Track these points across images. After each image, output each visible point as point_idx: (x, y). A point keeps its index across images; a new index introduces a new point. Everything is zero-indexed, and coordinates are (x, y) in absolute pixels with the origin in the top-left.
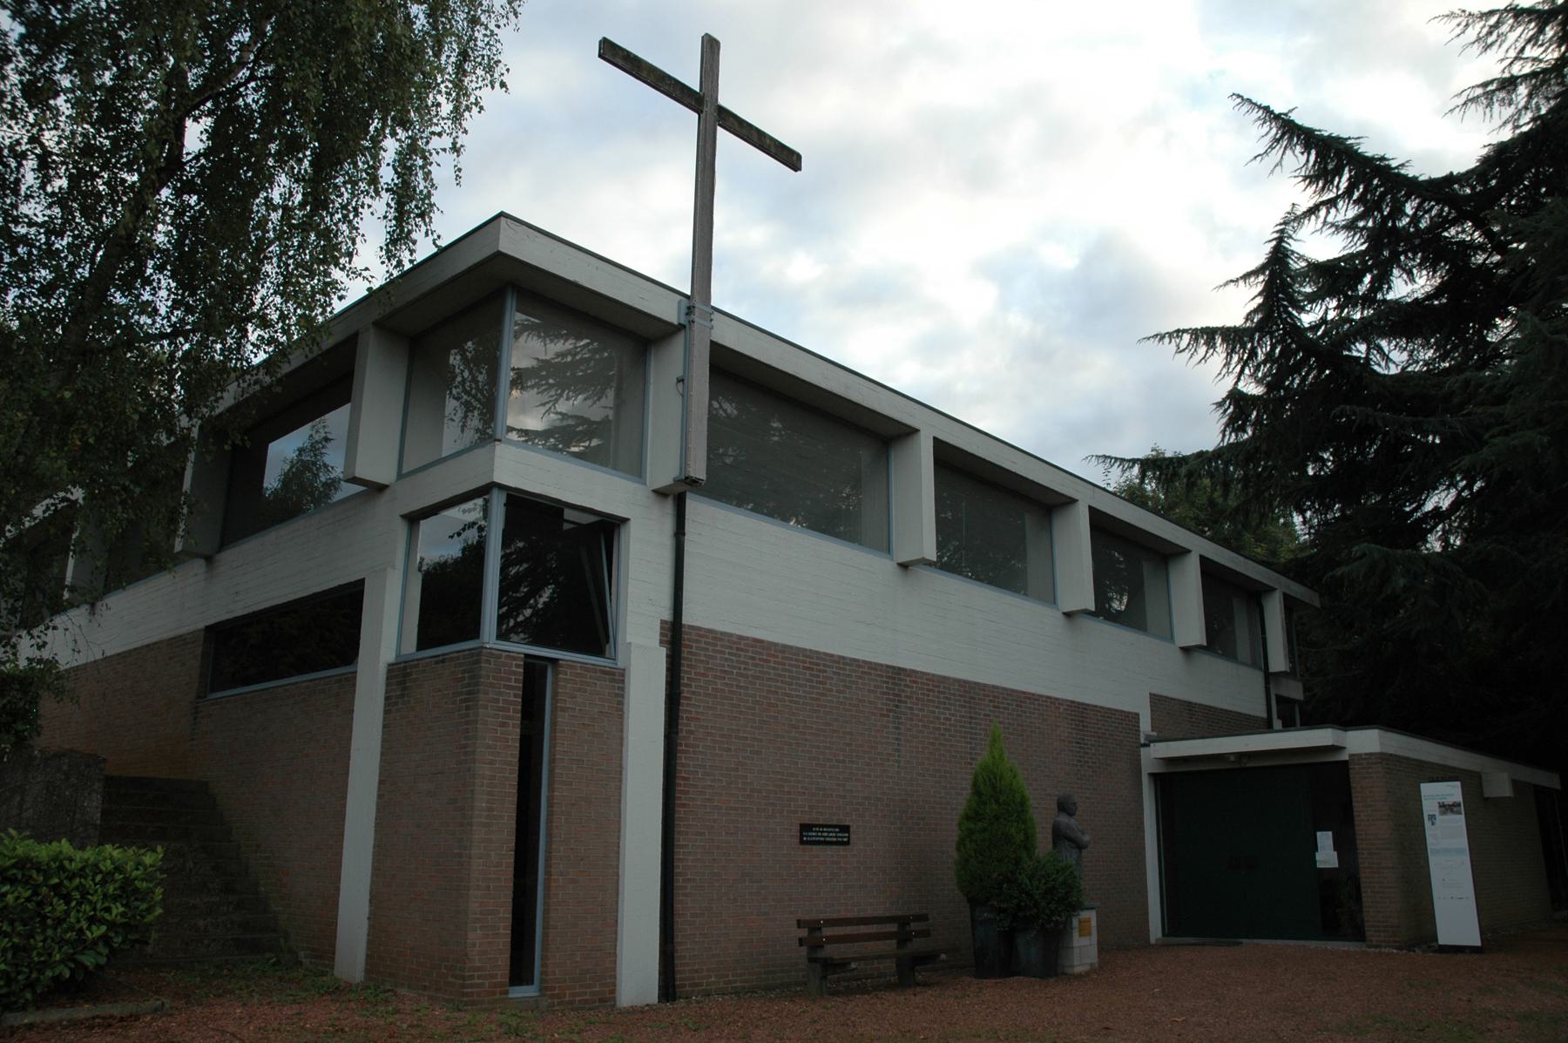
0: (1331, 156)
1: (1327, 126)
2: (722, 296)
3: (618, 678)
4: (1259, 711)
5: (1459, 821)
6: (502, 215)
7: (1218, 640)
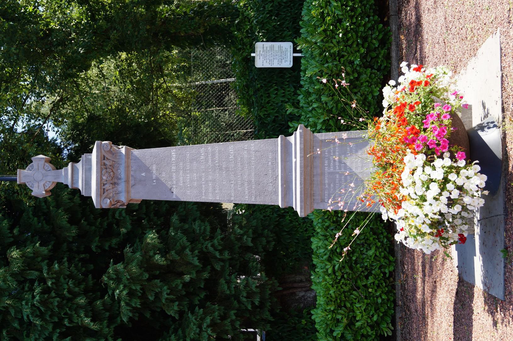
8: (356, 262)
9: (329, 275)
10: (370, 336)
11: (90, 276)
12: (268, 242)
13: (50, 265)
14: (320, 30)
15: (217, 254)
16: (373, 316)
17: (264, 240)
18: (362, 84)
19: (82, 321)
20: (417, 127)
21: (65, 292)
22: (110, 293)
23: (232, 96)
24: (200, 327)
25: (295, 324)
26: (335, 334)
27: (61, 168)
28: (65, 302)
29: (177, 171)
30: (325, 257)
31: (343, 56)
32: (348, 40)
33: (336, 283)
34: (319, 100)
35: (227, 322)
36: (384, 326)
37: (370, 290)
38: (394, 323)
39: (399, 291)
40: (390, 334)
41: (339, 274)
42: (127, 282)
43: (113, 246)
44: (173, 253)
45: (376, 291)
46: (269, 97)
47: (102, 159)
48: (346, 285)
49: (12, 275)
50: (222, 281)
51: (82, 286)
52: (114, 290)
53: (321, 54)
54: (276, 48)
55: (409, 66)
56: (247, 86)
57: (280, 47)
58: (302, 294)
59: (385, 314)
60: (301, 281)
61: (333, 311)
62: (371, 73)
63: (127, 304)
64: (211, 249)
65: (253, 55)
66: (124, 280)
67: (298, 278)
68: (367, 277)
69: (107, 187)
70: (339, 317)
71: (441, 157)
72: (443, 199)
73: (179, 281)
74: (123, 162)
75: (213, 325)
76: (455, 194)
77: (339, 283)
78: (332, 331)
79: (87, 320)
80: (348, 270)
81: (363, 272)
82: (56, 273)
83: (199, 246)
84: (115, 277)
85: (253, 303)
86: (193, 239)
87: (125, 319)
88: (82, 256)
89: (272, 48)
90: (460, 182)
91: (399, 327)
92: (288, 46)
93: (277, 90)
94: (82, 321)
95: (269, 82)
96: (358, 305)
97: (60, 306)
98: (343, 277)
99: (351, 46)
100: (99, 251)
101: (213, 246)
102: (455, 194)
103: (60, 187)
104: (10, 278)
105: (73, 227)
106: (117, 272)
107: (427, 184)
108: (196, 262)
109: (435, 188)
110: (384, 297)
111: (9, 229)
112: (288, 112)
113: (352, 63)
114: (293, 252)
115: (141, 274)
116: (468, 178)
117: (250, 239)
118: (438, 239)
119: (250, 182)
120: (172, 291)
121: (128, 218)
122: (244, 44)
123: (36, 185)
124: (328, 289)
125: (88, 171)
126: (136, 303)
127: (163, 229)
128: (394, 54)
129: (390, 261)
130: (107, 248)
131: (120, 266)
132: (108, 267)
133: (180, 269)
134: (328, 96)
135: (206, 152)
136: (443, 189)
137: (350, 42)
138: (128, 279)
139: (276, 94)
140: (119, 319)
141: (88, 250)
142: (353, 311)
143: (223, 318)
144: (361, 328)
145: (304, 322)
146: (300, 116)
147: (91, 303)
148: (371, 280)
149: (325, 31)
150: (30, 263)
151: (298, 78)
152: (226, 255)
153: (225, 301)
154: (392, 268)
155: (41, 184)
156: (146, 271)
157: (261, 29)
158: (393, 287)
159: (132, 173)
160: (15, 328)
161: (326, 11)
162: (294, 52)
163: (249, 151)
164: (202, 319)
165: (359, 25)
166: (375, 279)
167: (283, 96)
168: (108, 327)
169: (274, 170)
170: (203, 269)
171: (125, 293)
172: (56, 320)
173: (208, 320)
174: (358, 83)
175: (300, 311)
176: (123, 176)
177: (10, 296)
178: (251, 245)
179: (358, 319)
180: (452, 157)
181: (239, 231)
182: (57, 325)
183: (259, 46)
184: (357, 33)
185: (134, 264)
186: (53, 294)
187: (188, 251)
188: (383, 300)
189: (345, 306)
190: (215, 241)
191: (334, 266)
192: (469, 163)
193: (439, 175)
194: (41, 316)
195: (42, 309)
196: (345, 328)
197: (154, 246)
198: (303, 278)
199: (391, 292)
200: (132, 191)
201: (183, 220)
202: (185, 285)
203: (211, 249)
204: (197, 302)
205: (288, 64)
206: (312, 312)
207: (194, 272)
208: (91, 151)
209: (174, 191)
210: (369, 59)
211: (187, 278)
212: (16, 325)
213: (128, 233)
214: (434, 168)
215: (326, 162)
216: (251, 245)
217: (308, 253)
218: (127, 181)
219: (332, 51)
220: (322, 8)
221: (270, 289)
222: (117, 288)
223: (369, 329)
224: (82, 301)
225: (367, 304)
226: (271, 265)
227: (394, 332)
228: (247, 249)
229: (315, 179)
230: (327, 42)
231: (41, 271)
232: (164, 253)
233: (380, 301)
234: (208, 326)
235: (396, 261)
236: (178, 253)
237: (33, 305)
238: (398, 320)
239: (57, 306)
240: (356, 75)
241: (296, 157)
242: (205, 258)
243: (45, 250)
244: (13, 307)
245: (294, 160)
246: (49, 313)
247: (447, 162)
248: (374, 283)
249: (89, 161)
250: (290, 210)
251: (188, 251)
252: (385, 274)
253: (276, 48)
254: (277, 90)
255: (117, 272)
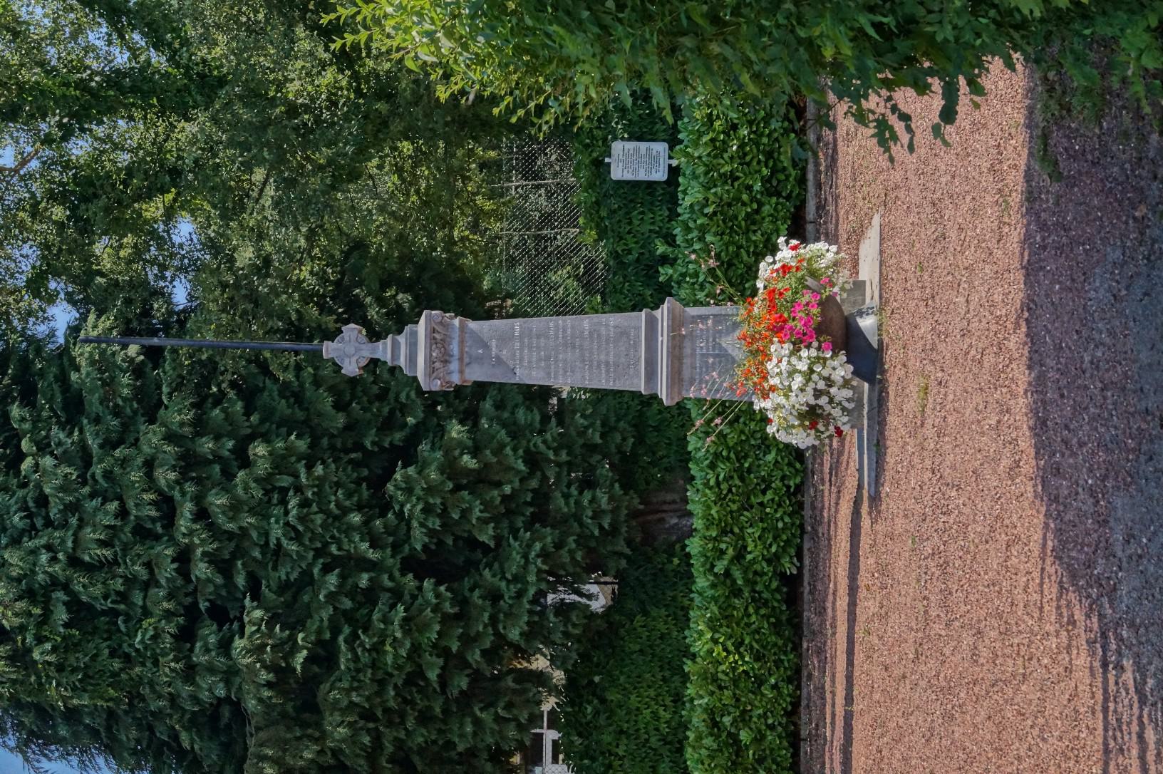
8: (749, 471)
9: (711, 488)
10: (766, 574)
11: (364, 485)
12: (624, 439)
13: (310, 467)
14: (705, 139)
15: (551, 455)
16: (770, 545)
17: (618, 438)
18: (763, 218)
19: (355, 548)
20: (786, 315)
21: (332, 506)
22: (397, 508)
23: (553, 157)
24: (525, 556)
25: (664, 564)
26: (716, 570)
27: (377, 340)
28: (330, 520)
29: (521, 349)
30: (707, 462)
31: (738, 178)
32: (745, 154)
33: (720, 498)
34: (701, 239)
35: (564, 552)
36: (785, 561)
37: (768, 510)
38: (799, 555)
39: (807, 512)
40: (795, 572)
41: (724, 486)
42: (421, 493)
43: (397, 443)
44: (488, 452)
45: (776, 511)
46: (630, 223)
47: (431, 332)
48: (734, 502)
49: (256, 481)
50: (558, 494)
51: (355, 499)
52: (402, 506)
53: (706, 173)
54: (643, 151)
55: (787, 242)
56: (597, 203)
58: (675, 521)
59: (788, 542)
60: (674, 502)
61: (715, 539)
62: (777, 204)
63: (422, 525)
64: (542, 447)
65: (607, 160)
66: (418, 491)
67: (669, 497)
68: (764, 492)
69: (437, 365)
70: (723, 546)
71: (808, 347)
72: (809, 390)
73: (496, 493)
75: (544, 554)
76: (821, 385)
77: (724, 499)
78: (713, 566)
79: (364, 546)
80: (738, 482)
81: (758, 484)
82: (318, 478)
83: (524, 443)
84: (404, 485)
85: (601, 528)
86: (515, 433)
87: (419, 547)
88: (353, 456)
90: (825, 373)
91: (807, 561)
92: (660, 148)
93: (642, 213)
94: (355, 548)
95: (631, 201)
96: (750, 531)
97: (324, 525)
98: (730, 491)
99: (748, 164)
100: (376, 449)
101: (545, 442)
102: (821, 385)
103: (374, 362)
104: (253, 485)
105: (340, 414)
106: (407, 479)
107: (791, 373)
108: (521, 466)
109: (798, 380)
110: (787, 519)
111: (244, 414)
112: (658, 252)
113: (749, 188)
114: (662, 458)
115: (443, 482)
116: (834, 369)
117: (597, 435)
118: (813, 432)
119: (607, 364)
120: (487, 506)
121: (419, 401)
122: (593, 138)
123: (347, 361)
124: (709, 508)
125: (413, 346)
126: (435, 523)
127: (470, 417)
128: (810, 176)
129: (797, 470)
130: (386, 445)
131: (411, 470)
132: (395, 472)
133: (497, 478)
134: (716, 234)
135: (557, 326)
136: (809, 380)
137: (748, 158)
138: (423, 489)
140: (407, 548)
141: (359, 446)
142: (744, 539)
143: (559, 545)
144: (754, 560)
145: (676, 561)
146: (675, 259)
147: (367, 522)
148: (769, 495)
149: (713, 140)
150: (280, 463)
151: (674, 202)
152: (564, 457)
153: (561, 523)
154: (798, 480)
155: (354, 359)
156: (449, 479)
157: (622, 118)
158: (801, 505)
160: (254, 559)
161: (715, 112)
163: (607, 325)
164: (529, 546)
165: (762, 135)
166: (775, 493)
167: (653, 223)
168: (393, 556)
170: (531, 474)
171: (419, 507)
172: (319, 545)
173: (538, 546)
174: (757, 217)
175: (672, 545)
176: (1050, 535)
177: (252, 511)
178: (600, 441)
179: (749, 549)
180: (819, 349)
181: (582, 421)
182: (319, 553)
183: (617, 147)
184: (757, 144)
185: (433, 468)
186: (314, 508)
187: (508, 450)
188: (785, 524)
189: (732, 532)
190: (548, 436)
191: (718, 476)
192: (835, 354)
193: (803, 366)
194: (298, 537)
195: (301, 528)
196: (731, 561)
197: (460, 443)
198: (676, 497)
199: (797, 513)
200: (467, 371)
201: (499, 406)
202: (505, 498)
203: (542, 447)
204: (521, 525)
205: (660, 175)
206: (687, 542)
207: (517, 480)
208: (417, 322)
209: (517, 371)
210: (775, 183)
211: (507, 489)
212: (257, 554)
213: (417, 425)
214: (800, 358)
216: (600, 441)
217: (685, 458)
218: (461, 359)
219: (722, 171)
220: (709, 107)
221: (627, 508)
222: (407, 501)
223: (764, 564)
224: (356, 518)
225: (764, 529)
226: (627, 473)
227: (800, 569)
228: (591, 448)
230: (715, 157)
231: (297, 476)
232: (476, 452)
233: (780, 525)
234: (538, 556)
235: (805, 470)
236: (494, 453)
237: (287, 524)
238: (806, 552)
239: (321, 526)
240: (755, 206)
242: (534, 461)
243: (302, 445)
244: (256, 528)
246: (309, 535)
247: (813, 353)
248: (773, 500)
249: (414, 334)
250: (654, 397)
251: (508, 450)
252: (788, 487)
253: (643, 151)
254: (642, 213)
255: (407, 479)
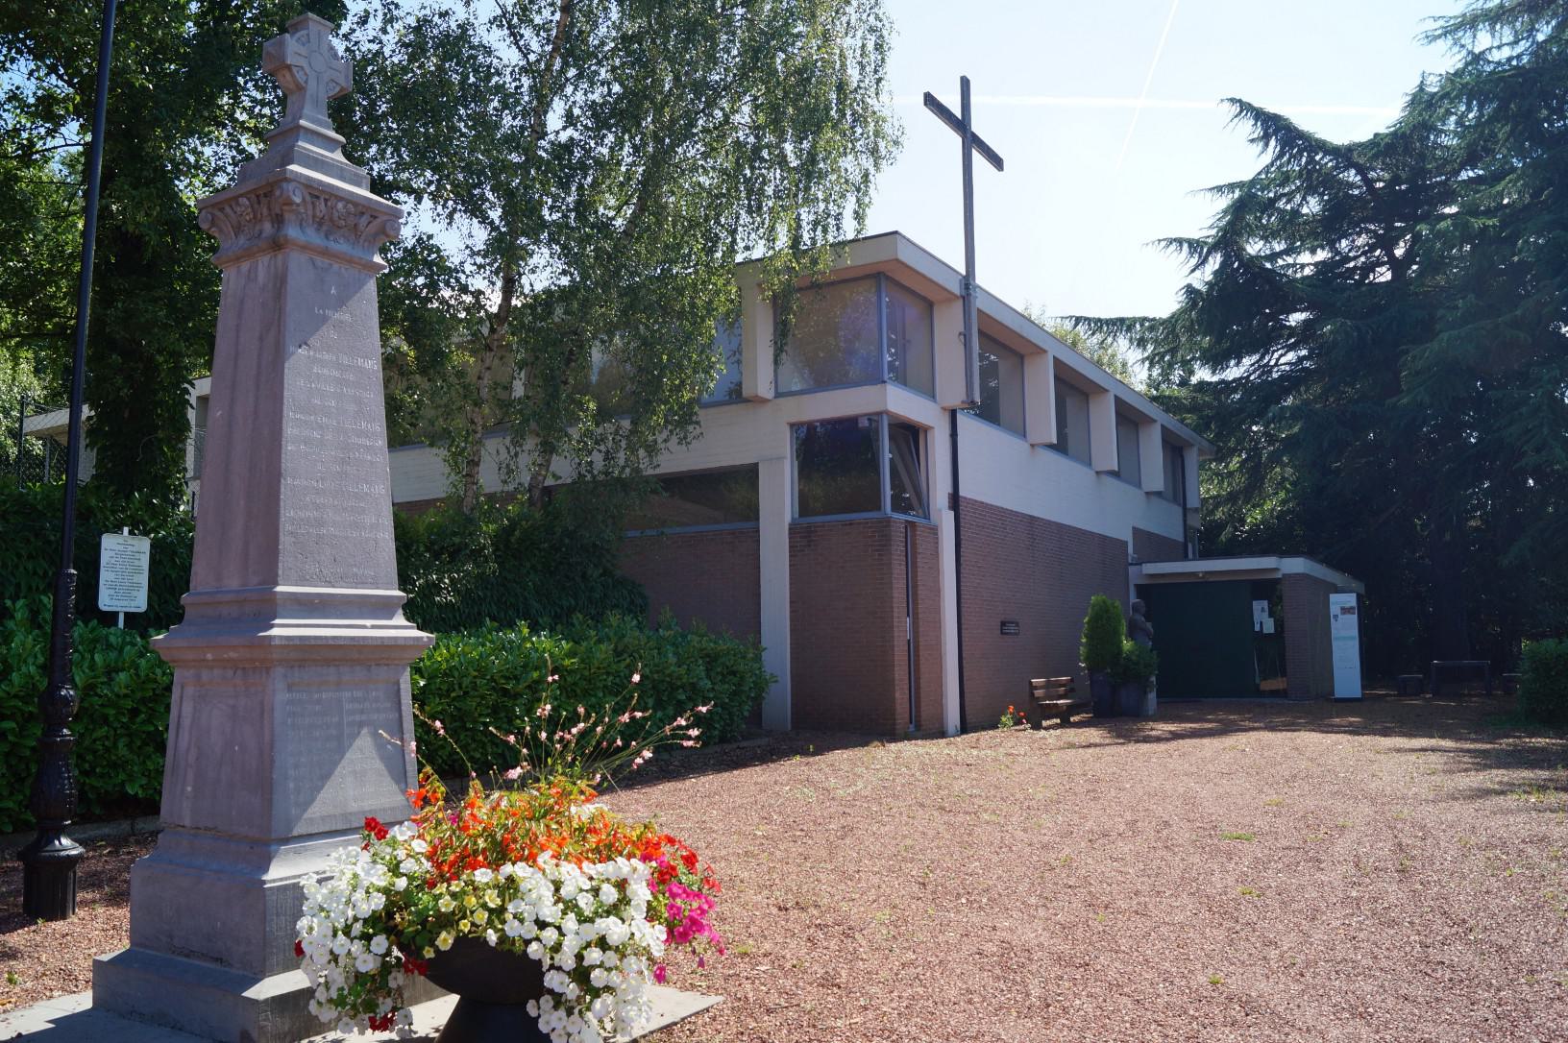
0: (1273, 127)
1: (1271, 108)
2: (981, 279)
3: (934, 531)
4: (1176, 534)
5: (1353, 619)
6: (896, 232)
7: (1126, 472)
46: (30, 557)
57: (139, 586)
65: (126, 530)
69: (321, 206)
74: (357, 253)
89: (138, 570)
93: (45, 573)
139: (35, 573)
155: (303, 63)
159: (336, 266)
162: (127, 614)
169: (343, 580)
205: (106, 601)
215: (359, 694)
229: (332, 670)
241: (373, 627)
245: (369, 622)
